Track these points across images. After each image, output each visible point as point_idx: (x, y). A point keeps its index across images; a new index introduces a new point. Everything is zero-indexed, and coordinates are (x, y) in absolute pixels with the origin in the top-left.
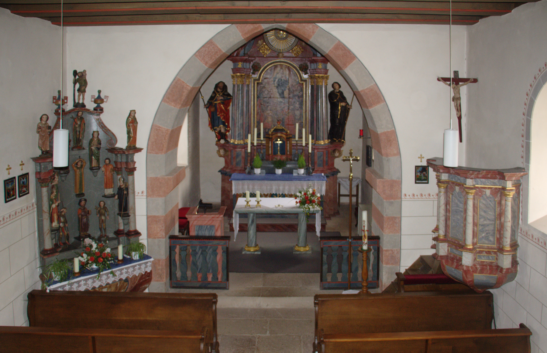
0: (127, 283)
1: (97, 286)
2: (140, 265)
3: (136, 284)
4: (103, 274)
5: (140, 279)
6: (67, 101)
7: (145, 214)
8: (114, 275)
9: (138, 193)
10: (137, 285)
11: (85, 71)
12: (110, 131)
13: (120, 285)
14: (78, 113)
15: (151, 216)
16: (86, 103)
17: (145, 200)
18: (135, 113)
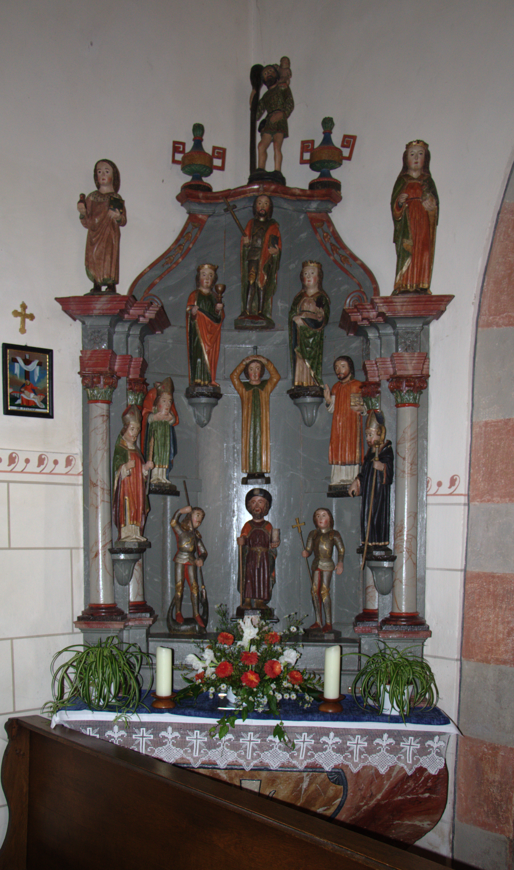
0: (341, 787)
1: (222, 765)
2: (397, 735)
3: (373, 802)
4: (247, 729)
5: (392, 792)
6: (223, 163)
7: (460, 564)
8: (290, 747)
9: (439, 484)
10: (378, 805)
11: (285, 60)
12: (355, 258)
13: (313, 787)
14: (255, 202)
15: (478, 576)
16: (285, 172)
17: (461, 512)
18: (289, 64)
